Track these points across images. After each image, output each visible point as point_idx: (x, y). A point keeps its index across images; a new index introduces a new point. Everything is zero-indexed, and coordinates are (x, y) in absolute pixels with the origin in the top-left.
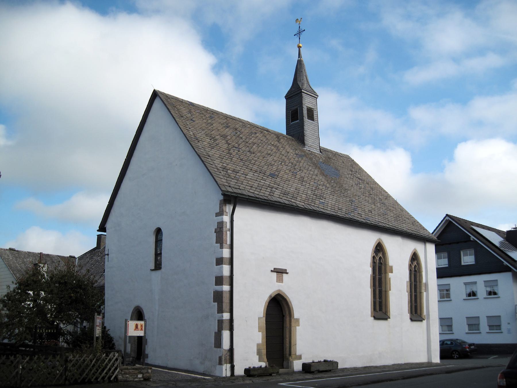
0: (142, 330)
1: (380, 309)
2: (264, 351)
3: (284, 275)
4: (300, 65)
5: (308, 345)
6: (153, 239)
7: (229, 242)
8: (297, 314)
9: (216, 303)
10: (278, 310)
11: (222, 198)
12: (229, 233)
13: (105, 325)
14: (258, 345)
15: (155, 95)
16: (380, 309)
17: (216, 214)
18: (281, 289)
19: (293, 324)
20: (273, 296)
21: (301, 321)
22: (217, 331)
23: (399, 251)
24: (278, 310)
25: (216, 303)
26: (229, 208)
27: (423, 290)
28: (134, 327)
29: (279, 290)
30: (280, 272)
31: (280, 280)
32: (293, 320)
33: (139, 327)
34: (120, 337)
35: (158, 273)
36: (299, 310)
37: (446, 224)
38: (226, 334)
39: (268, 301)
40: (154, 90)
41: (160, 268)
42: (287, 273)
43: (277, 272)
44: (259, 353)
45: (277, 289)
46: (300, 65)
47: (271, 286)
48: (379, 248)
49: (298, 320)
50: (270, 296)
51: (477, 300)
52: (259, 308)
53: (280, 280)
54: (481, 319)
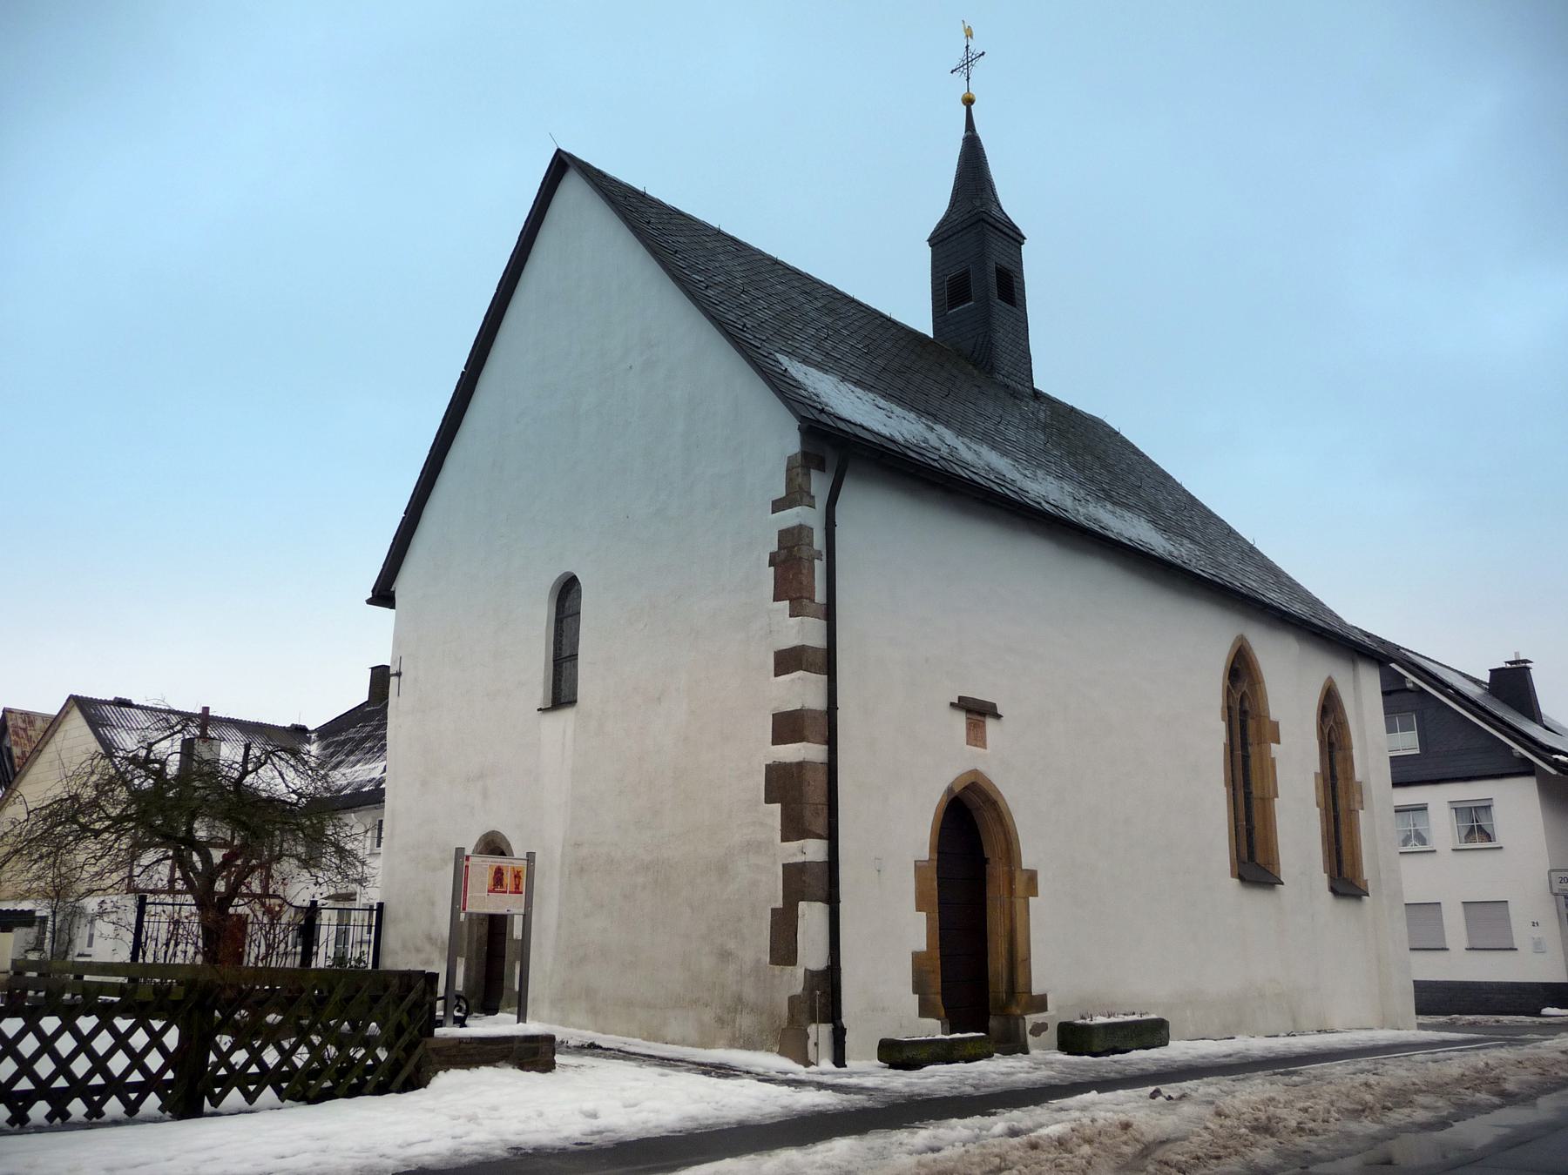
0: (517, 891)
1: (1254, 863)
3: (990, 724)
4: (973, 160)
6: (541, 614)
7: (820, 596)
9: (777, 807)
11: (791, 443)
12: (820, 567)
14: (917, 957)
15: (562, 165)
16: (1254, 863)
17: (774, 503)
18: (981, 768)
22: (779, 904)
23: (1291, 681)
25: (777, 807)
26: (819, 485)
27: (1014, 1078)
28: (488, 879)
29: (975, 772)
30: (977, 712)
31: (976, 736)
32: (1018, 874)
33: (508, 879)
34: (430, 939)
35: (566, 716)
36: (1037, 841)
37: (1374, 646)
38: (812, 916)
39: (944, 805)
40: (559, 150)
41: (572, 702)
42: (999, 717)
43: (969, 711)
44: (919, 987)
45: (966, 766)
46: (973, 160)
47: (947, 759)
48: (1241, 671)
50: (950, 790)
51: (1497, 853)
53: (976, 736)
54: (1513, 909)
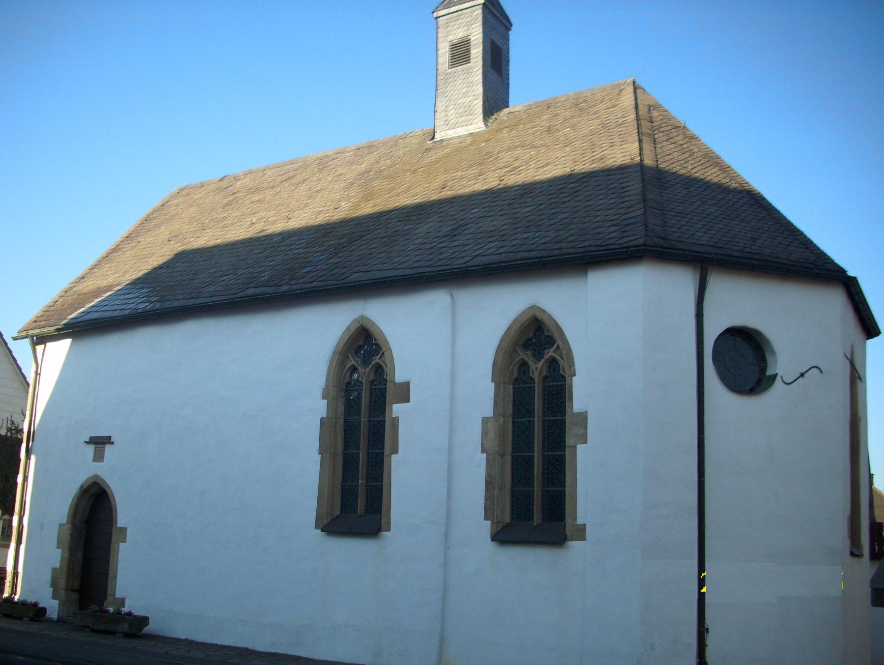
2: (62, 583)
5: (136, 582)
8: (122, 519)
10: (93, 518)
13: (878, 520)
14: (54, 570)
16: (356, 499)
18: (99, 473)
19: (114, 538)
20: (85, 487)
21: (129, 533)
24: (93, 518)
29: (96, 476)
30: (100, 443)
36: (125, 515)
43: (96, 443)
44: (54, 584)
47: (83, 469)
49: (123, 530)
52: (61, 510)
53: (99, 457)
